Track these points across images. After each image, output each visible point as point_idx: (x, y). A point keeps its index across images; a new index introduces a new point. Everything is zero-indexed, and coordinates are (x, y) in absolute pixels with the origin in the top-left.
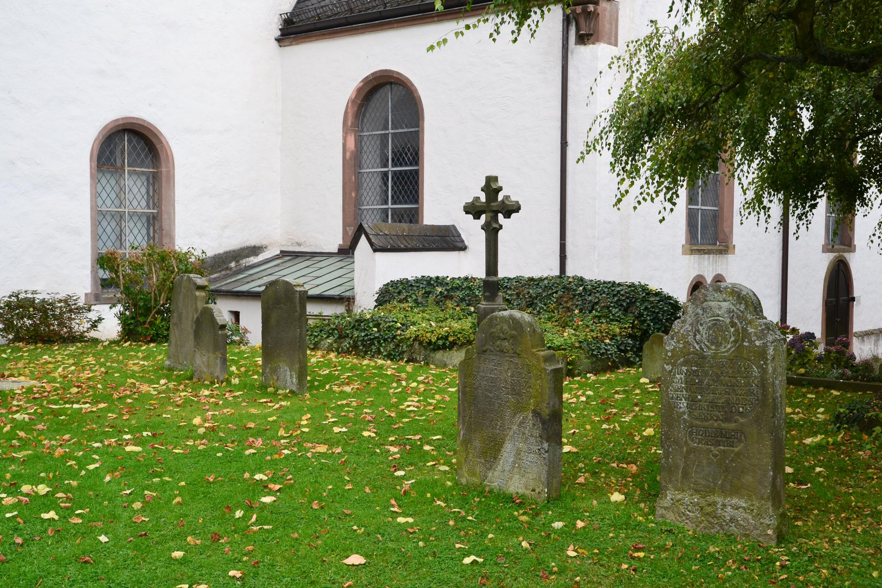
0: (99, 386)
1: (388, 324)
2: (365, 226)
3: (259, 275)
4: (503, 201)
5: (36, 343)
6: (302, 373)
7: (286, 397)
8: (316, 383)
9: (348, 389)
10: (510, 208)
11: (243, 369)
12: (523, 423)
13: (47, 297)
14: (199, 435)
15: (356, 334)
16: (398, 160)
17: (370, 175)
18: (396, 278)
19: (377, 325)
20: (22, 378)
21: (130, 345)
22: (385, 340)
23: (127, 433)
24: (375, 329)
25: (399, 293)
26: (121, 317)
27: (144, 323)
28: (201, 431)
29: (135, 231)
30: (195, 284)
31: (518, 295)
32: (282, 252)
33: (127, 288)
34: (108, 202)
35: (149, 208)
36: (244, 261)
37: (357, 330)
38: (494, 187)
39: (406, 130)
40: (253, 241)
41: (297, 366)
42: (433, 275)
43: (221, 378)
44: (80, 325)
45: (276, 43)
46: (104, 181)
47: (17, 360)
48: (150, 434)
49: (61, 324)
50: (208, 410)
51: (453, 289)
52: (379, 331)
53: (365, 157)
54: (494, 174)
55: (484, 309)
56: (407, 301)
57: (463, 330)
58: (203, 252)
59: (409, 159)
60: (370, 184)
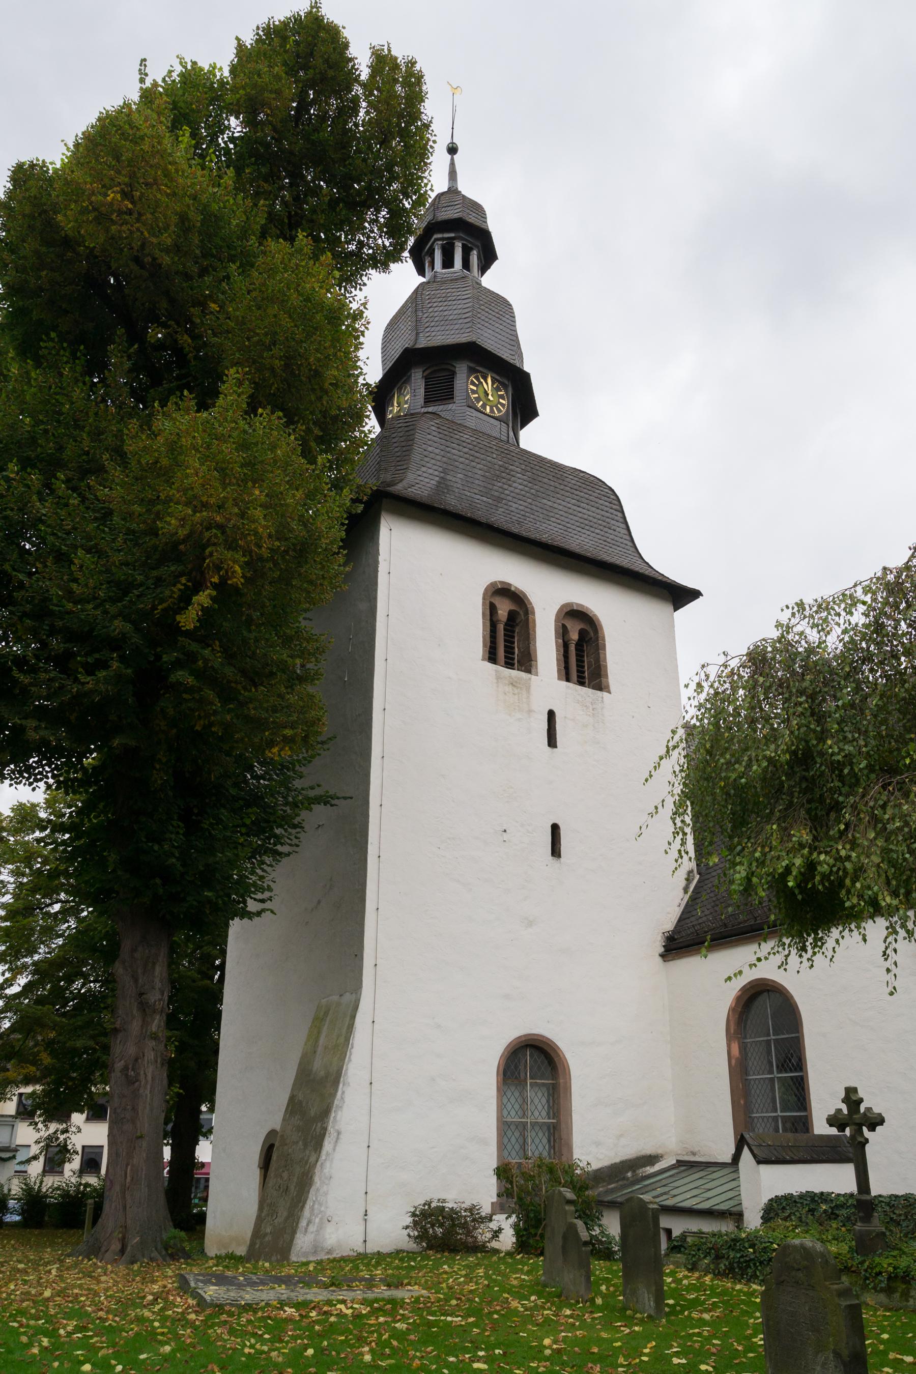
0: (477, 1299)
1: (764, 1245)
2: (747, 1136)
3: (654, 1186)
4: (865, 1113)
5: (444, 1252)
6: (660, 1296)
7: (641, 1322)
8: (678, 1308)
9: (706, 1316)
10: (843, 1122)
11: (612, 1289)
12: (826, 1364)
13: (455, 1206)
14: (545, 1356)
15: (732, 1254)
16: (783, 1065)
17: (757, 1082)
18: (780, 1193)
19: (752, 1246)
20: (416, 1287)
21: (522, 1257)
22: (761, 1263)
23: (482, 1350)
24: (751, 1250)
25: (784, 1208)
26: (515, 1226)
27: (536, 1235)
28: (548, 1352)
29: (537, 1141)
30: (565, 1198)
31: (906, 1215)
32: (678, 1161)
33: (520, 1199)
34: (513, 1113)
35: (549, 1118)
36: (641, 1170)
37: (733, 1250)
38: (854, 1098)
39: (787, 1036)
40: (648, 1150)
41: (654, 1288)
42: (817, 1191)
43: (586, 1298)
44: (483, 1234)
45: (660, 959)
46: (509, 1094)
47: (420, 1269)
48: (501, 1352)
49: (469, 1233)
50: (562, 1331)
51: (837, 1206)
52: (754, 1252)
53: (750, 1064)
54: (853, 1085)
55: (859, 1230)
56: (791, 1220)
57: (840, 1254)
58: (588, 1164)
59: (793, 1065)
60: (758, 1091)
